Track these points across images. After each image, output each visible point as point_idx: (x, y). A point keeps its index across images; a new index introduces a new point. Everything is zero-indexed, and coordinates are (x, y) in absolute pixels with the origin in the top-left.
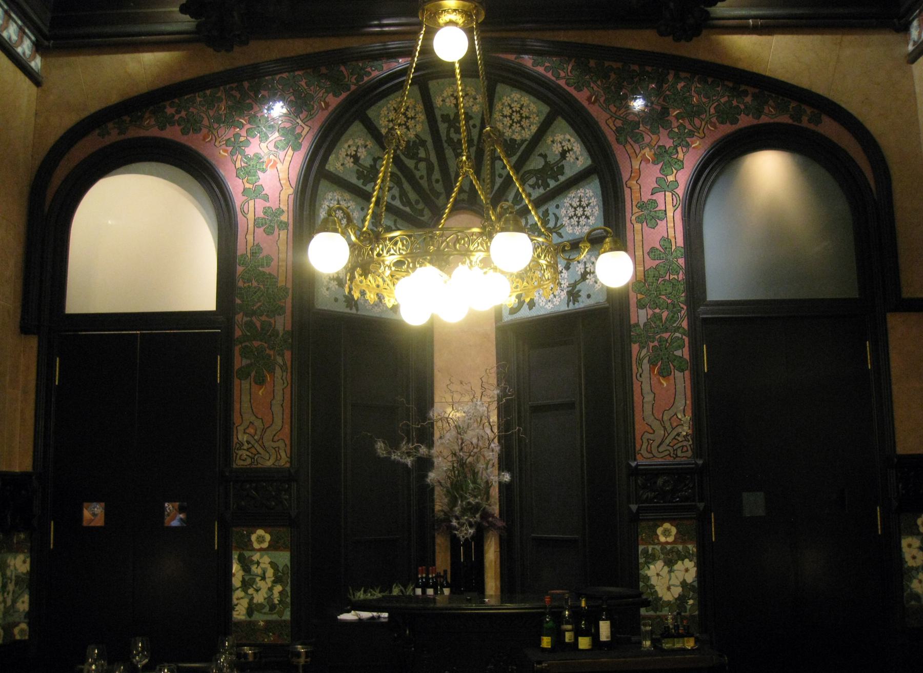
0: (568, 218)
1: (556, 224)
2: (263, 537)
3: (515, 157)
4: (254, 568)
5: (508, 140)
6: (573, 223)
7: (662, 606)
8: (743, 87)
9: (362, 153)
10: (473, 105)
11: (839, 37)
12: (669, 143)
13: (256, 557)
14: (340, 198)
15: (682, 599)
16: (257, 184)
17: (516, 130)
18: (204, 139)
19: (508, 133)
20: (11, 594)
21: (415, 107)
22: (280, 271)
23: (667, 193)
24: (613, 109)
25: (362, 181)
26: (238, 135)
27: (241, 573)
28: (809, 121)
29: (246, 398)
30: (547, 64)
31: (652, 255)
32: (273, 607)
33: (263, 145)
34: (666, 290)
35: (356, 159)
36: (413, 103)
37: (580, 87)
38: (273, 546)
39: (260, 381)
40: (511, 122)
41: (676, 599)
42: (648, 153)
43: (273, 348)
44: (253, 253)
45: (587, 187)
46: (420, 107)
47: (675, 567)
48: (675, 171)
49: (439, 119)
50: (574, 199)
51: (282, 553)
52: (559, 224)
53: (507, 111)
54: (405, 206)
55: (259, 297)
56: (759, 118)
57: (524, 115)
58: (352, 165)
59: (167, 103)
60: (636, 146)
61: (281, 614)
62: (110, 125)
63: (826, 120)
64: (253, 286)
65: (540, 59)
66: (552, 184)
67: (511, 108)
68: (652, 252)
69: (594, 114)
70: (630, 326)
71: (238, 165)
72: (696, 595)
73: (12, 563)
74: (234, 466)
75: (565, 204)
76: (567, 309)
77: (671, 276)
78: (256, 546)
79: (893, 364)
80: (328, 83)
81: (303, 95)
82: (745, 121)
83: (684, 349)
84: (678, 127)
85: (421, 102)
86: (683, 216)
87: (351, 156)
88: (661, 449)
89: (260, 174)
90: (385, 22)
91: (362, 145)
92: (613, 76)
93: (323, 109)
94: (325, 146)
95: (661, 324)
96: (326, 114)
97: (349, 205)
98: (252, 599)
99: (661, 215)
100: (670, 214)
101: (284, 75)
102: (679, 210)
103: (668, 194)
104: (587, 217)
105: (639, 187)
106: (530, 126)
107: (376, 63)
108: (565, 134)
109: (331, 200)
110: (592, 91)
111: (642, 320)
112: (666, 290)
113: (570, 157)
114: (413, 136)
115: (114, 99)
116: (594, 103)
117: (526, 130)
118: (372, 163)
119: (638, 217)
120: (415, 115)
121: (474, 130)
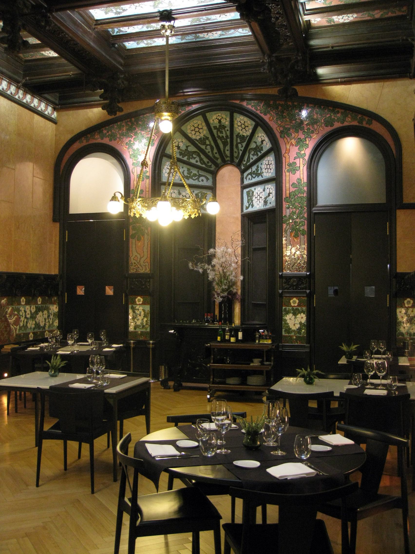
2: (140, 299)
4: (136, 311)
7: (291, 332)
8: (337, 110)
9: (181, 145)
11: (382, 83)
12: (302, 137)
13: (137, 307)
15: (300, 329)
18: (118, 142)
19: (241, 133)
20: (51, 320)
21: (201, 124)
23: (301, 159)
24: (279, 123)
25: (182, 156)
26: (130, 141)
27: (132, 313)
28: (366, 124)
29: (134, 246)
30: (252, 104)
31: (293, 186)
32: (143, 327)
33: (140, 145)
35: (178, 147)
38: (144, 303)
39: (139, 240)
41: (297, 329)
42: (293, 141)
46: (204, 124)
47: (297, 316)
49: (213, 128)
51: (147, 306)
53: (239, 124)
56: (343, 123)
59: (104, 129)
60: (288, 139)
61: (146, 329)
62: (83, 138)
63: (374, 122)
66: (259, 154)
67: (241, 123)
69: (271, 125)
71: (131, 153)
72: (306, 328)
73: (52, 308)
74: (130, 272)
78: (137, 303)
79: (398, 233)
82: (337, 125)
84: (307, 129)
85: (204, 122)
86: (307, 169)
88: (293, 268)
92: (280, 108)
94: (244, 112)
98: (136, 323)
99: (298, 169)
100: (301, 168)
102: (306, 166)
103: (301, 159)
104: (271, 169)
107: (183, 108)
115: (84, 128)
116: (271, 121)
119: (288, 170)
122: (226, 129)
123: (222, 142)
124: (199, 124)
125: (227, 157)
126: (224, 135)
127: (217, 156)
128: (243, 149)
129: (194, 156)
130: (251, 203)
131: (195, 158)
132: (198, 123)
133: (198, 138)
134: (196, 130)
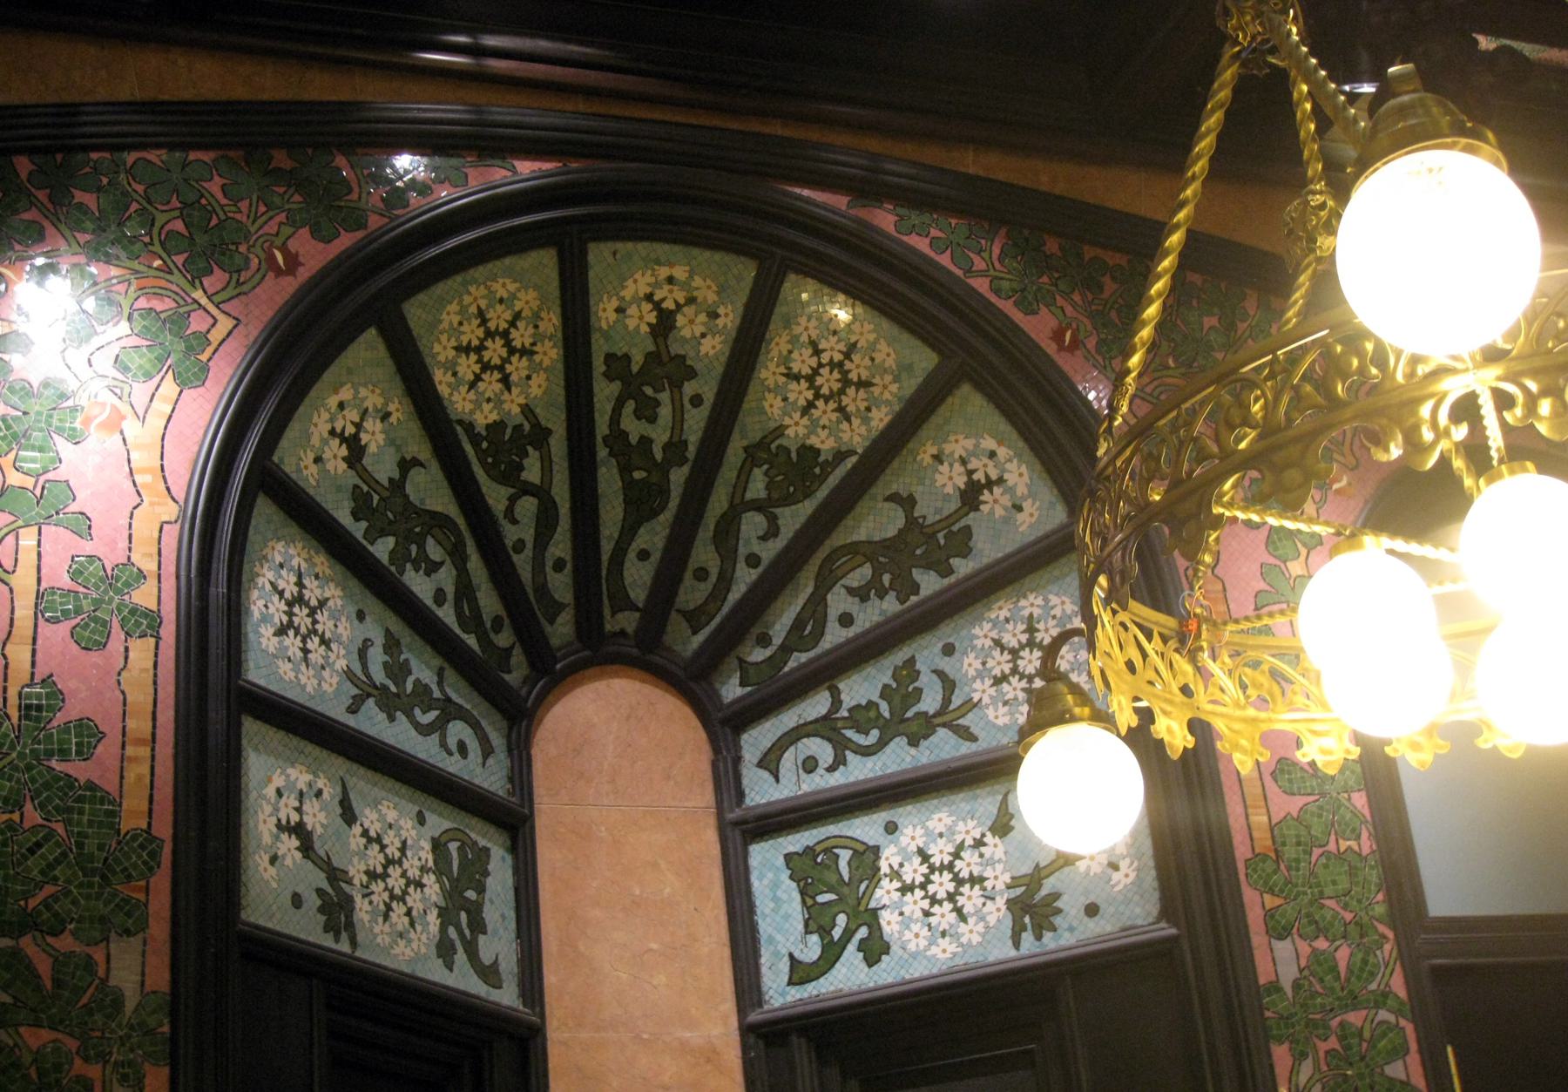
0: (988, 682)
1: (947, 701)
3: (807, 503)
5: (793, 450)
6: (1010, 696)
9: (374, 437)
10: (703, 335)
14: (304, 565)
16: (50, 476)
17: (824, 421)
19: (796, 431)
21: (537, 316)
22: (130, 776)
25: (364, 524)
30: (934, 232)
34: (1334, 883)
35: (355, 451)
36: (535, 304)
37: (1030, 304)
40: (810, 395)
43: (103, 1057)
44: (29, 707)
45: (1055, 588)
46: (552, 321)
48: (1304, 551)
49: (599, 366)
50: (1010, 627)
52: (957, 701)
54: (468, 633)
55: (51, 867)
57: (853, 376)
58: (343, 466)
64: (26, 825)
65: (915, 218)
68: (1282, 771)
70: (1258, 987)
75: (978, 643)
76: (1013, 953)
77: (1341, 841)
80: (297, 198)
81: (214, 222)
83: (1408, 1059)
87: (344, 439)
89: (63, 446)
90: (491, 41)
91: (377, 410)
93: (279, 272)
95: (1337, 985)
96: (288, 286)
97: (327, 594)
101: (153, 156)
105: (1220, 587)
106: (868, 409)
108: (978, 436)
109: (281, 566)
110: (1061, 317)
111: (1289, 976)
112: (1334, 883)
113: (994, 503)
114: (516, 410)
117: (856, 422)
118: (396, 475)
120: (534, 344)
121: (694, 411)
122: (689, 388)
123: (629, 485)
124: (517, 316)
125: (622, 602)
126: (660, 435)
127: (561, 585)
128: (769, 551)
129: (434, 551)
130: (848, 934)
131: (433, 568)
132: (518, 305)
133: (485, 417)
134: (487, 355)
